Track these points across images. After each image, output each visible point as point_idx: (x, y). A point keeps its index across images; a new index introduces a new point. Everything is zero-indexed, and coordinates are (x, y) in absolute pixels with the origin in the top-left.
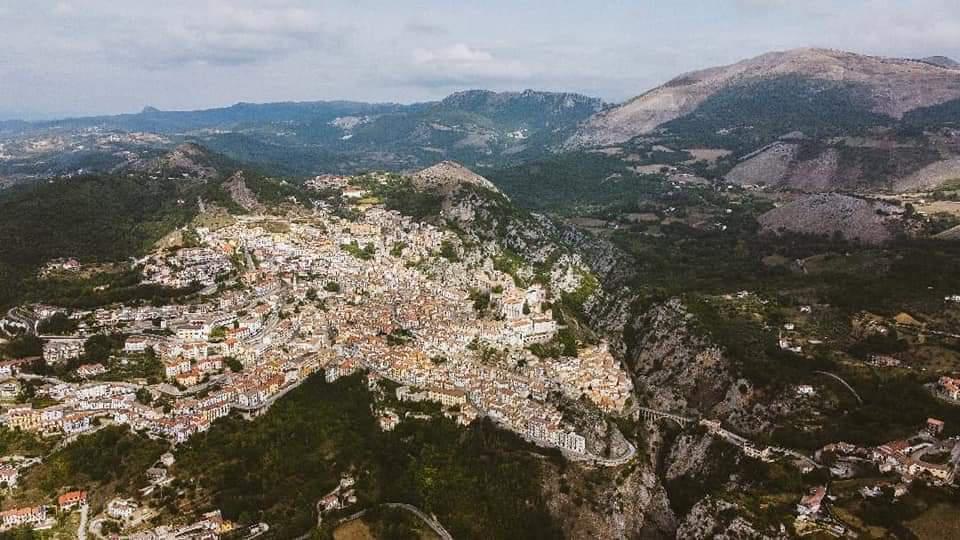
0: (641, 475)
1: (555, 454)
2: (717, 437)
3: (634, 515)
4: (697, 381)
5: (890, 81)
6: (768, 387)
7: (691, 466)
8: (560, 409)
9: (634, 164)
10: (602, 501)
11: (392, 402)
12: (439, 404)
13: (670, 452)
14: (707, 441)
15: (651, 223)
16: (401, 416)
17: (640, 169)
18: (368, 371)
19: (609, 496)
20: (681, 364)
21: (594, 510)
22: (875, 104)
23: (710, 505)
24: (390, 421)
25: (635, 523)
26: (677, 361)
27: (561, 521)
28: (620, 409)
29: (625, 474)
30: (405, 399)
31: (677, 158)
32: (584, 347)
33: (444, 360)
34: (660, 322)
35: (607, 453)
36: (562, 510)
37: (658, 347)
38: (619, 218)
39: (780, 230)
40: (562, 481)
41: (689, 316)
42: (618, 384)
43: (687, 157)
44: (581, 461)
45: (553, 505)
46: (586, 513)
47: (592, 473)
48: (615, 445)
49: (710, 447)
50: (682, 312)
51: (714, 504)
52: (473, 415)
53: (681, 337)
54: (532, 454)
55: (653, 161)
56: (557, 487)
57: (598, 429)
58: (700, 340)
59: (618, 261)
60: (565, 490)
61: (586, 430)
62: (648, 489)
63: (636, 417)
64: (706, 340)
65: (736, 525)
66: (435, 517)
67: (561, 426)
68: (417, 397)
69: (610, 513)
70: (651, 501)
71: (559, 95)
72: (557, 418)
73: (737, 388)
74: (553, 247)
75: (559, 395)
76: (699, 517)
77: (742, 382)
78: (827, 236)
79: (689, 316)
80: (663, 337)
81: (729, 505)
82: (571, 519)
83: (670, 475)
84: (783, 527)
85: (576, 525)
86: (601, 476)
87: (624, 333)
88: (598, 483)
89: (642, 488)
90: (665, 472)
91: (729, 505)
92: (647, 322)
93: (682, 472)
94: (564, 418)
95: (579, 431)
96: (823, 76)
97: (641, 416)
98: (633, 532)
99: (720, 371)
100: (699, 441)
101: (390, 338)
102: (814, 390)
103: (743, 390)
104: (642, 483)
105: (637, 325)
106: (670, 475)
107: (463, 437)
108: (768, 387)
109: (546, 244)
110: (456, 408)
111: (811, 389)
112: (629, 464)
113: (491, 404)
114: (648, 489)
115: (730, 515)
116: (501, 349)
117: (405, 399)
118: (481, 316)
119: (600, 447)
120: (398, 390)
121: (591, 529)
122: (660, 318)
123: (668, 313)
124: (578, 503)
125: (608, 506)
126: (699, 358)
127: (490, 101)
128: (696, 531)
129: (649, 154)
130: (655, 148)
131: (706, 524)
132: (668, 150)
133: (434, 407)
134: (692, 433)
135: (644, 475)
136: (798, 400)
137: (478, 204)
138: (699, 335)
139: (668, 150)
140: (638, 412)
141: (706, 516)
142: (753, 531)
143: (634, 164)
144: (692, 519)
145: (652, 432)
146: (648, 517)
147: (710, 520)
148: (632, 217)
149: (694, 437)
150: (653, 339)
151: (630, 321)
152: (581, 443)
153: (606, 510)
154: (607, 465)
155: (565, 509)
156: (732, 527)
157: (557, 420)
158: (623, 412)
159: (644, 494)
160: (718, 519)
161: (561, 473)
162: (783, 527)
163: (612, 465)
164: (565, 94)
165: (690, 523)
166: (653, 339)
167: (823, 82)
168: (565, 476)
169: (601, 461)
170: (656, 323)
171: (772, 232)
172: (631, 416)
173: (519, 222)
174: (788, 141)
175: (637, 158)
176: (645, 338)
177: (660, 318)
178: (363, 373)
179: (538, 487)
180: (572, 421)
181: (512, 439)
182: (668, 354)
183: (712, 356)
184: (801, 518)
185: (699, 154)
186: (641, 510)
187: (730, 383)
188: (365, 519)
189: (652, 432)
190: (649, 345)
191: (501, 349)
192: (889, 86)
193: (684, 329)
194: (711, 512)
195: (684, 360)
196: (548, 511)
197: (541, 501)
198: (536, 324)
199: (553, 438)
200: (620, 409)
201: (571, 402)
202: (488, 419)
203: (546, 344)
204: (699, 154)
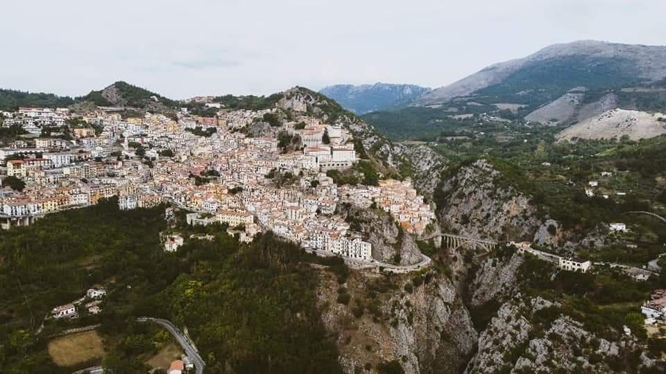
0: (437, 286)
1: (337, 264)
2: (528, 256)
3: (427, 334)
4: (504, 228)
5: (651, 56)
6: (577, 227)
7: (499, 290)
8: (348, 220)
9: (453, 114)
10: (385, 309)
11: (184, 229)
12: (226, 225)
13: (475, 277)
14: (516, 262)
15: (464, 141)
16: (186, 238)
17: (457, 117)
18: (169, 205)
19: (396, 303)
20: (488, 215)
21: (375, 321)
22: (640, 72)
23: (523, 305)
24: (174, 244)
25: (430, 343)
26: (485, 214)
27: (336, 335)
28: (420, 233)
29: (417, 283)
30: (194, 223)
31: (489, 109)
32: (384, 179)
33: (240, 190)
34: (468, 180)
35: (397, 260)
36: (340, 322)
37: (466, 202)
38: (438, 140)
39: (573, 139)
40: (341, 291)
41: (495, 172)
42: (419, 209)
43: (494, 108)
44: (365, 269)
45: (329, 319)
46: (366, 323)
47: (377, 281)
48: (408, 251)
49: (520, 268)
50: (488, 170)
51: (528, 303)
52: (253, 232)
53: (488, 191)
54: (312, 265)
55: (468, 112)
56: (336, 296)
57: (387, 233)
58: (506, 192)
59: (436, 161)
60: (344, 299)
61: (373, 236)
62: (446, 304)
63: (438, 243)
64: (512, 191)
65: (560, 326)
66: (186, 331)
67: (348, 236)
68: (206, 221)
69: (395, 325)
70: (450, 318)
71: (400, 86)
72: (343, 228)
73: (545, 228)
74: (375, 139)
75: (347, 206)
76: (509, 319)
77: (554, 223)
78: (616, 139)
79: (495, 172)
80: (470, 194)
81: (548, 304)
82: (348, 333)
83: (475, 302)
84: (627, 330)
85: (353, 340)
86: (388, 283)
87: (434, 196)
88: (383, 291)
89: (440, 302)
90: (470, 301)
91: (548, 304)
92: (455, 185)
93: (487, 298)
94: (351, 229)
95: (366, 238)
96: (597, 55)
97: (444, 242)
98: (428, 351)
99: (526, 218)
100: (507, 262)
101: (197, 178)
102: (627, 228)
103: (552, 230)
104: (439, 295)
105: (445, 189)
106: (475, 302)
107: (241, 251)
108: (577, 227)
109: (370, 136)
110: (241, 228)
111: (624, 226)
112: (422, 272)
113: (276, 221)
114: (446, 304)
115: (549, 316)
116: (296, 172)
117: (194, 223)
118: (285, 152)
119: (388, 253)
120: (188, 215)
121: (370, 344)
122: (467, 176)
123: (475, 172)
124: (358, 314)
125: (393, 315)
126: (506, 207)
127: (350, 91)
128: (504, 338)
129: (465, 107)
130: (469, 104)
131: (517, 328)
132: (479, 105)
133: (221, 228)
134: (500, 255)
135: (441, 286)
136: (612, 235)
137: (311, 103)
138: (505, 189)
139: (479, 105)
140: (440, 239)
141: (518, 317)
142: (585, 333)
143: (453, 114)
144: (497, 323)
145: (455, 259)
146: (445, 337)
147: (523, 322)
148: (449, 138)
149: (501, 260)
150: (461, 196)
151: (440, 185)
152: (366, 249)
153: (391, 320)
154: (395, 271)
155: (344, 323)
156: (556, 329)
157: (343, 230)
158: (423, 235)
159: (440, 307)
160: (534, 322)
161: (341, 282)
162: (627, 330)
163: (402, 271)
164: (405, 85)
165: (496, 329)
166: (461, 196)
167: (596, 60)
168: (345, 285)
169: (389, 268)
170: (464, 181)
171: (566, 141)
172: (431, 241)
173: (346, 118)
174: (577, 92)
175: (455, 110)
176: (453, 196)
177: (467, 176)
178: (163, 206)
179: (314, 298)
180: (359, 230)
181: (294, 250)
182: (475, 208)
183: (518, 205)
184: (650, 321)
185: (503, 106)
186: (437, 328)
187: (537, 227)
188: (101, 332)
189: (455, 259)
190: (457, 201)
191: (296, 172)
192: (650, 60)
193: (490, 185)
194: (525, 313)
195: (491, 212)
196: (322, 324)
197: (315, 315)
198: (334, 152)
199: (334, 247)
200: (420, 233)
201: (359, 212)
202: (270, 233)
203: (345, 172)
204: (503, 106)
